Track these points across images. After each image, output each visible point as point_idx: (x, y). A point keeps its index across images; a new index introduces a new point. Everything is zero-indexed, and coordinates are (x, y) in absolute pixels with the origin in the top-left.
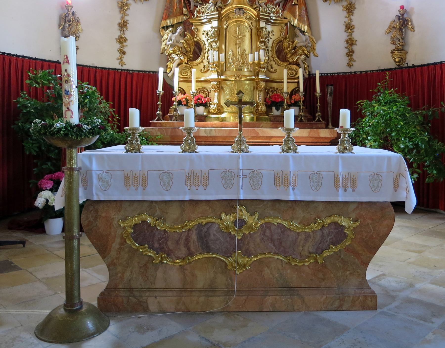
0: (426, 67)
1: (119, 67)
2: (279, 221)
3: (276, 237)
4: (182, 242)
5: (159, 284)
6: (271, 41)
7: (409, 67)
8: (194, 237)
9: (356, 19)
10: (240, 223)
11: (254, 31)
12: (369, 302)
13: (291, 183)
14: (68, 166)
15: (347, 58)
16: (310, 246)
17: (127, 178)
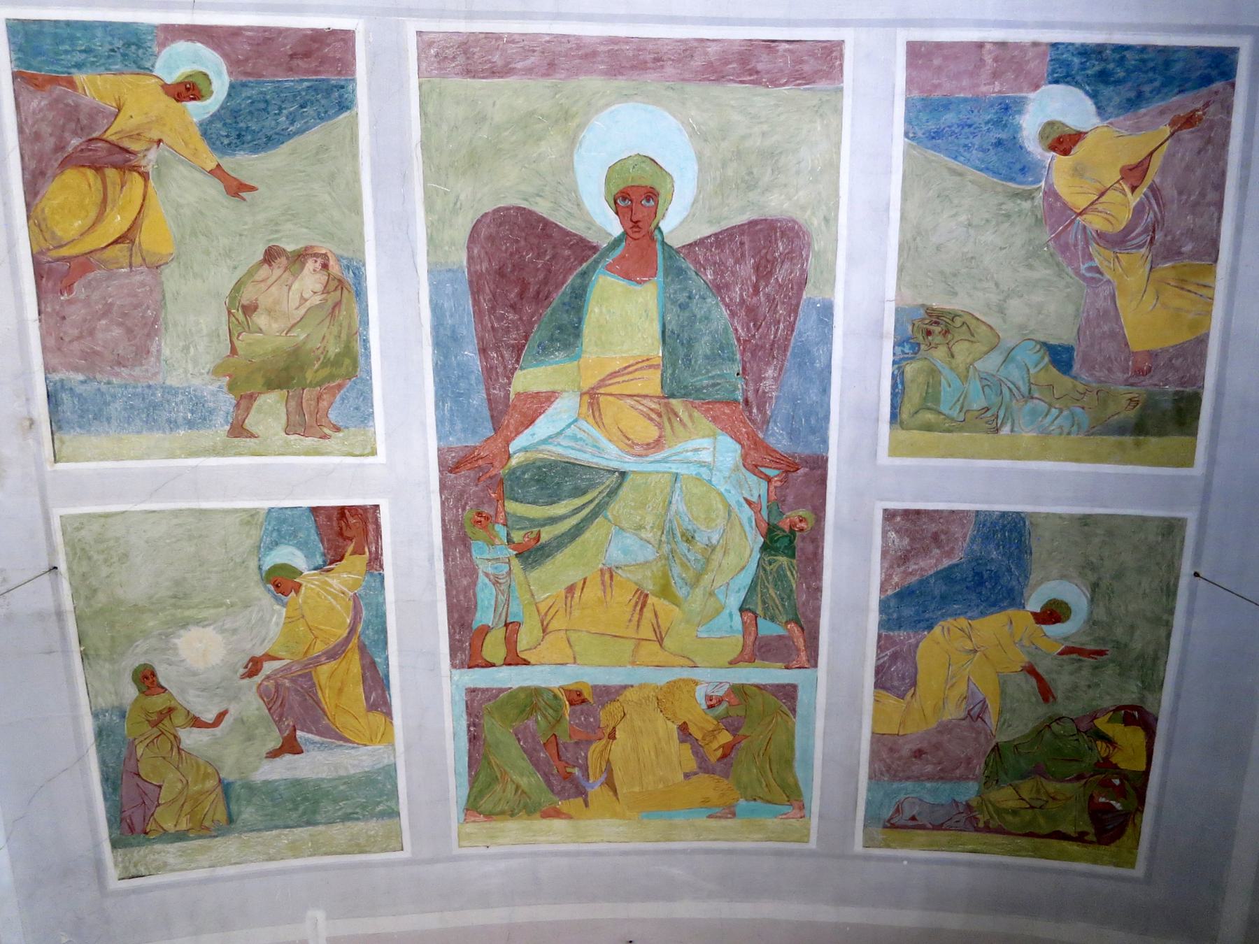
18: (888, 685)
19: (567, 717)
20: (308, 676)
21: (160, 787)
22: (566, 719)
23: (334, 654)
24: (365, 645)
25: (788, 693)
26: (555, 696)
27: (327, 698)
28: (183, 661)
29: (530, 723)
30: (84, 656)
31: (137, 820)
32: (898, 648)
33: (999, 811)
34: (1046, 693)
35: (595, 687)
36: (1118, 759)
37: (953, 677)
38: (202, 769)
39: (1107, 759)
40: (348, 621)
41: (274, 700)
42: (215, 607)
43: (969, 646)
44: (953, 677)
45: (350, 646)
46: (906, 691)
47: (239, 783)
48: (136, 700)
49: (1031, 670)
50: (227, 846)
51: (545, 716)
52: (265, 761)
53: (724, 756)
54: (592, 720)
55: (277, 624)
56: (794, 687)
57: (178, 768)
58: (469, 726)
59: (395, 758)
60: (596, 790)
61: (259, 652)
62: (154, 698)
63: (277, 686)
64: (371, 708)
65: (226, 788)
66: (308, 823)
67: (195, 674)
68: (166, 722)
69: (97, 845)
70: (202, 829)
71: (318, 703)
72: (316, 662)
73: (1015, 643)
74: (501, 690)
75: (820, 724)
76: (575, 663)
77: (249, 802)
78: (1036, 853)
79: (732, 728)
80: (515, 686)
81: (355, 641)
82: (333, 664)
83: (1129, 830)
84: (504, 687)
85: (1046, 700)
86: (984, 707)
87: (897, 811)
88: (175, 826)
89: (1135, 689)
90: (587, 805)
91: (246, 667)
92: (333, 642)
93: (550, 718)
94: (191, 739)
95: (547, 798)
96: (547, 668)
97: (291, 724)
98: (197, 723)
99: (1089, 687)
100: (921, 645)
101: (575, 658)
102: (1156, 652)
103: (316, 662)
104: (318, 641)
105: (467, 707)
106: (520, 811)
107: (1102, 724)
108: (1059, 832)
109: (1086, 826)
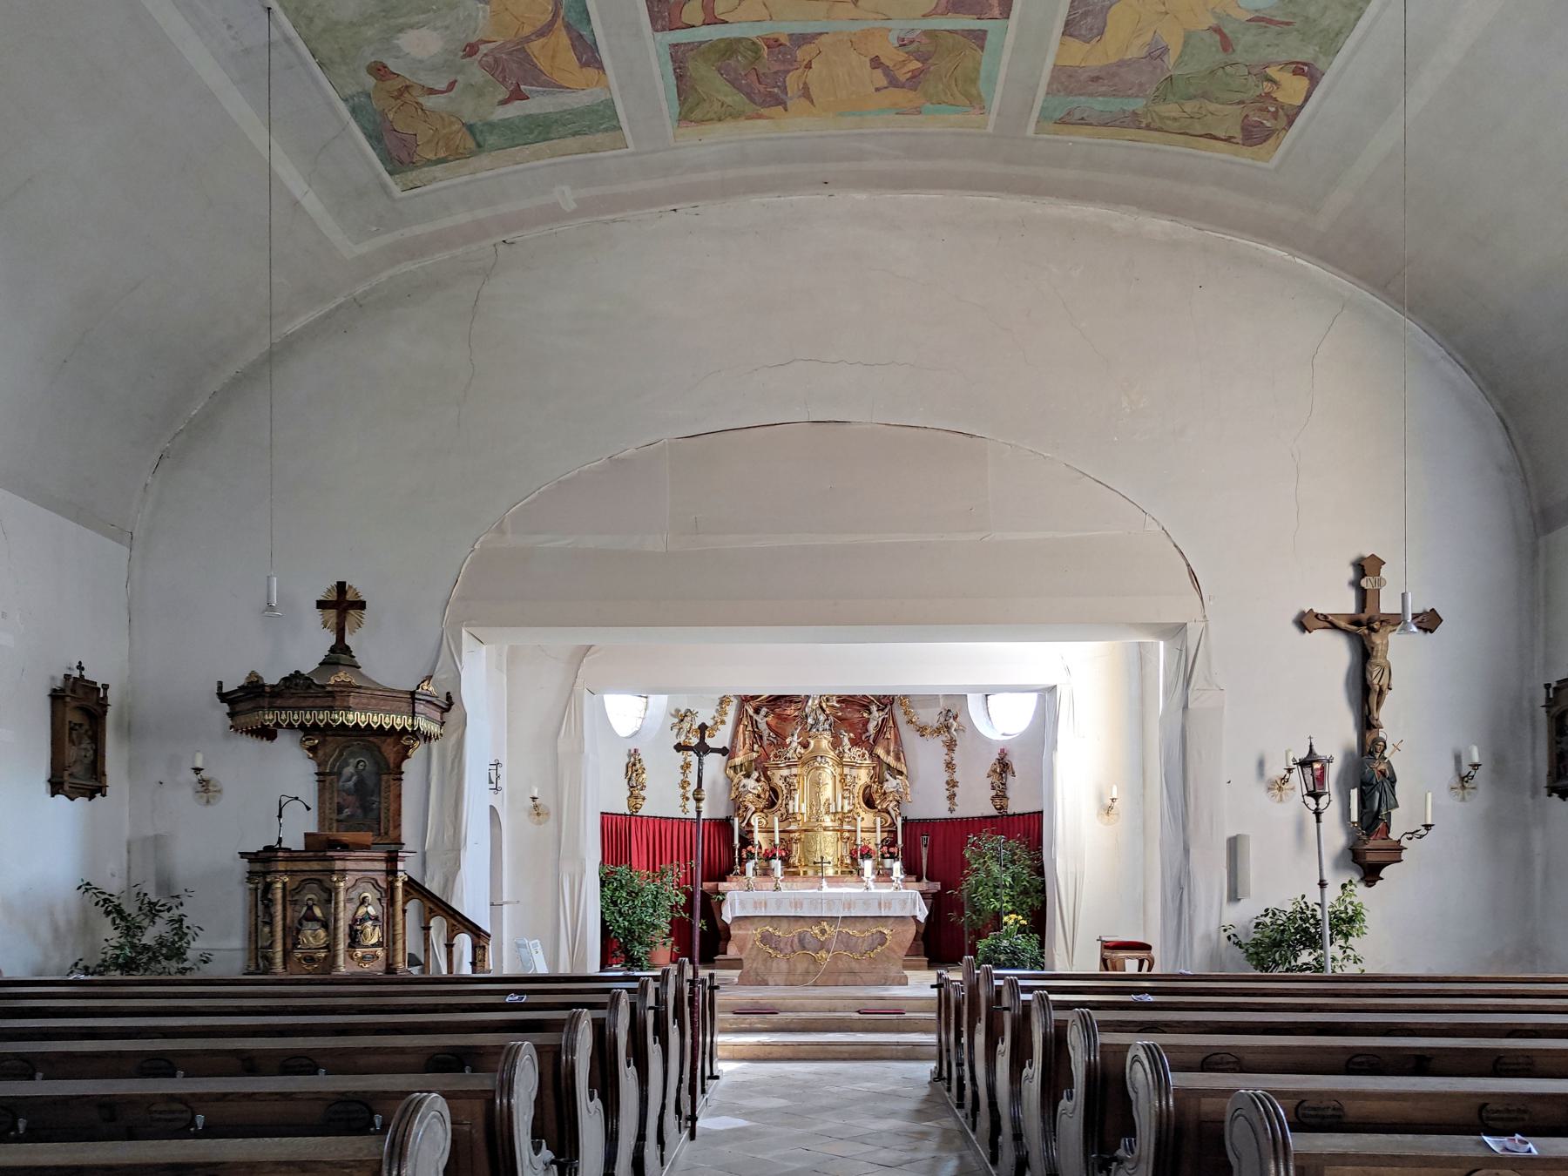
0: (1036, 815)
1: (682, 815)
2: (847, 930)
3: (844, 940)
4: (789, 944)
5: (774, 970)
6: (857, 787)
7: (1008, 815)
8: (796, 940)
9: (957, 757)
10: (823, 932)
11: (838, 778)
12: (903, 981)
13: (852, 906)
14: (1380, 660)
15: (949, 802)
16: (865, 947)
17: (755, 903)
18: (1076, 33)
19: (766, 56)
20: (523, 50)
21: (416, 135)
22: (764, 58)
23: (541, 33)
24: (570, 24)
25: (979, 37)
26: (754, 43)
27: (543, 63)
28: (408, 54)
29: (732, 62)
30: (320, 65)
31: (404, 156)
32: (1090, 8)
33: (1162, 118)
34: (1226, 45)
35: (791, 35)
36: (1280, 96)
37: (1140, 30)
38: (446, 119)
39: (1268, 94)
40: (550, 8)
41: (495, 68)
42: (423, 13)
43: (1163, 9)
44: (1140, 30)
45: (556, 26)
46: (1092, 38)
47: (480, 123)
48: (376, 86)
49: (1217, 30)
50: (484, 160)
51: (744, 57)
52: (497, 107)
53: (913, 77)
54: (789, 57)
55: (484, 18)
56: (985, 32)
57: (425, 121)
58: (675, 70)
59: (611, 94)
60: (795, 103)
61: (473, 39)
62: (388, 83)
63: (496, 60)
64: (585, 65)
65: (470, 128)
66: (545, 140)
67: (421, 61)
68: (406, 95)
69: (378, 176)
70: (457, 155)
71: (535, 66)
72: (528, 39)
73: (1207, 10)
74: (701, 43)
75: (1006, 57)
76: (771, 19)
77: (491, 133)
78: (1186, 145)
79: (922, 59)
80: (715, 38)
81: (559, 21)
82: (543, 40)
83: (1271, 141)
84: (703, 40)
85: (1225, 50)
86: (1166, 50)
87: (1068, 114)
88: (436, 155)
89: (1312, 52)
90: (786, 110)
91: (465, 50)
92: (539, 25)
93: (750, 58)
94: (429, 102)
95: (750, 108)
96: (745, 25)
97: (514, 82)
98: (432, 91)
99: (1269, 46)
100: (1113, 7)
101: (770, 16)
102: (1341, 28)
103: (528, 39)
104: (525, 26)
105: (672, 57)
106: (726, 117)
107: (1272, 72)
108: (1211, 134)
109: (1237, 132)
